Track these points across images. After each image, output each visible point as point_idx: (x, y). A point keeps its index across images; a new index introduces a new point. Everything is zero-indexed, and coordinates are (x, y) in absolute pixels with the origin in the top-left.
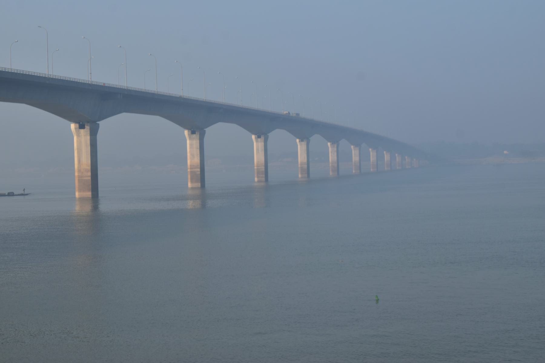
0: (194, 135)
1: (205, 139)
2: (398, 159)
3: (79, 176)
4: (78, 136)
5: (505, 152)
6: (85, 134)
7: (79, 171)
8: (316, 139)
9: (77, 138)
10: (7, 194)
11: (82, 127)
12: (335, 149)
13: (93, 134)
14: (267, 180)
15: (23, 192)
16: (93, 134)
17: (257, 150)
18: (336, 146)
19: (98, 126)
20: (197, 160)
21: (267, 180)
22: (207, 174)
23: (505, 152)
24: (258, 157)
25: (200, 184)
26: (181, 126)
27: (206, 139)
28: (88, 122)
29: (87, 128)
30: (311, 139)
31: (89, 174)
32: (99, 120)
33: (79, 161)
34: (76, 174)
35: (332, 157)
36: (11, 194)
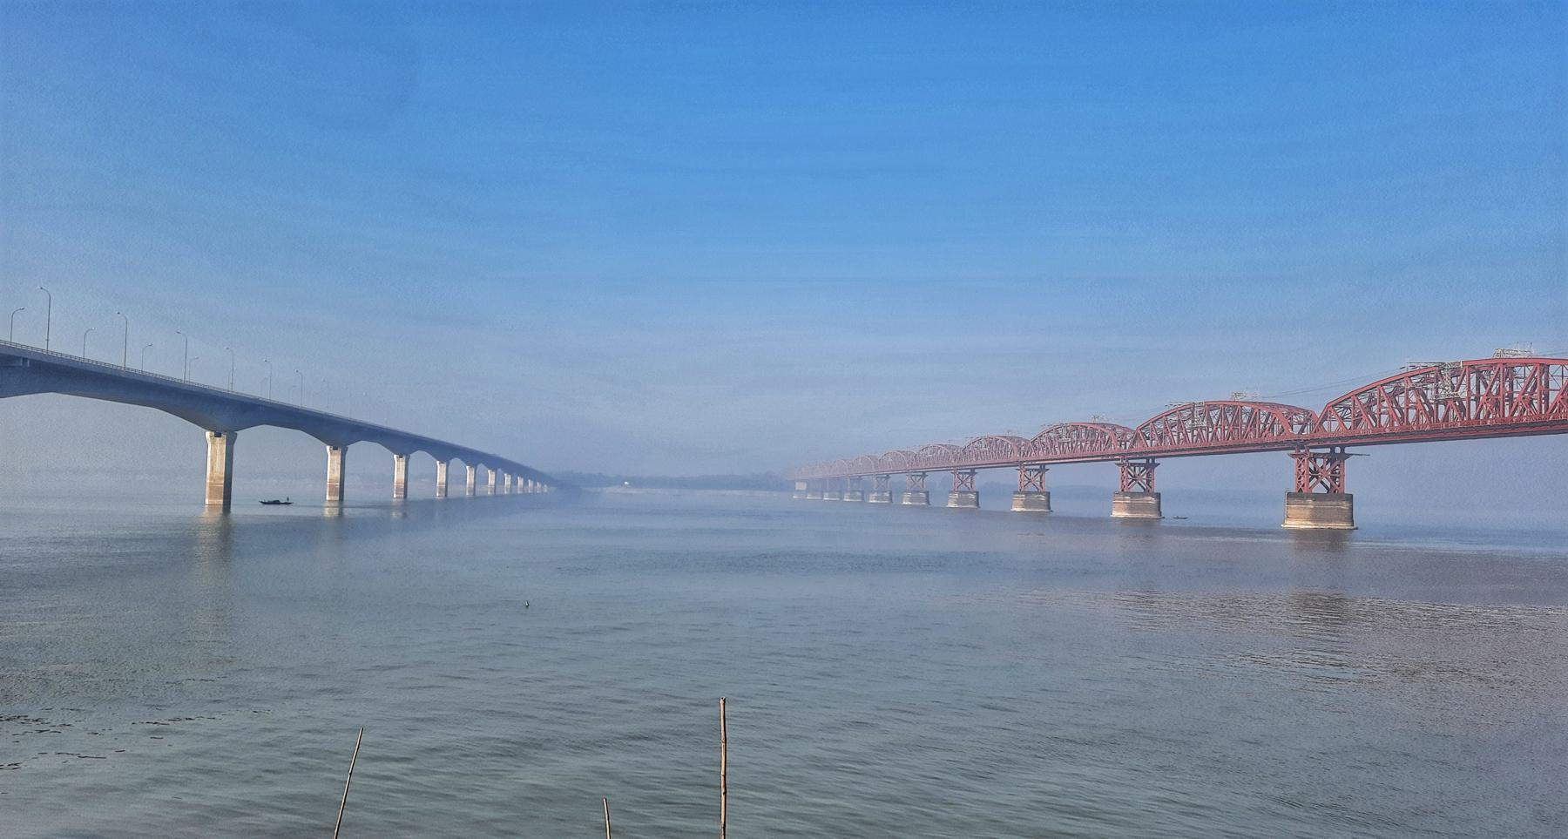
3: (210, 483)
5: (626, 483)
7: (211, 478)
8: (456, 462)
11: (218, 435)
13: (230, 444)
14: (446, 495)
16: (230, 444)
20: (337, 475)
21: (446, 495)
33: (212, 469)
34: (208, 481)
35: (470, 479)
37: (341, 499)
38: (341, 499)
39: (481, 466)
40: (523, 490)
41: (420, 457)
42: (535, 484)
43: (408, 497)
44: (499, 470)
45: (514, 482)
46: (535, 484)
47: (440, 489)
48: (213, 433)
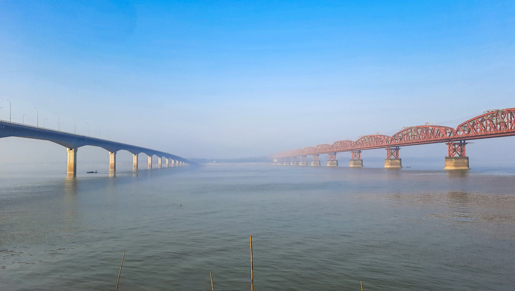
0: (71, 151)
1: (138, 157)
2: (181, 163)
3: (69, 166)
4: (69, 152)
5: (214, 161)
6: (72, 152)
7: (69, 165)
8: (155, 156)
9: (387, 168)
10: (393, 160)
11: (71, 149)
12: (161, 159)
13: (75, 152)
14: (151, 168)
15: (95, 172)
16: (75, 152)
17: (134, 159)
18: (161, 158)
19: (116, 153)
20: (113, 162)
21: (151, 168)
22: (116, 167)
23: (214, 161)
24: (135, 161)
25: (73, 172)
26: (108, 150)
27: (152, 158)
28: (73, 148)
29: (73, 150)
30: (153, 156)
31: (73, 166)
32: (78, 147)
33: (69, 161)
35: (160, 162)
36: (92, 172)
37: (115, 170)
38: (115, 170)
39: (163, 157)
40: (182, 165)
41: (142, 155)
42: (182, 163)
43: (138, 169)
44: (170, 158)
45: (170, 162)
46: (182, 163)
47: (149, 166)
48: (69, 149)
